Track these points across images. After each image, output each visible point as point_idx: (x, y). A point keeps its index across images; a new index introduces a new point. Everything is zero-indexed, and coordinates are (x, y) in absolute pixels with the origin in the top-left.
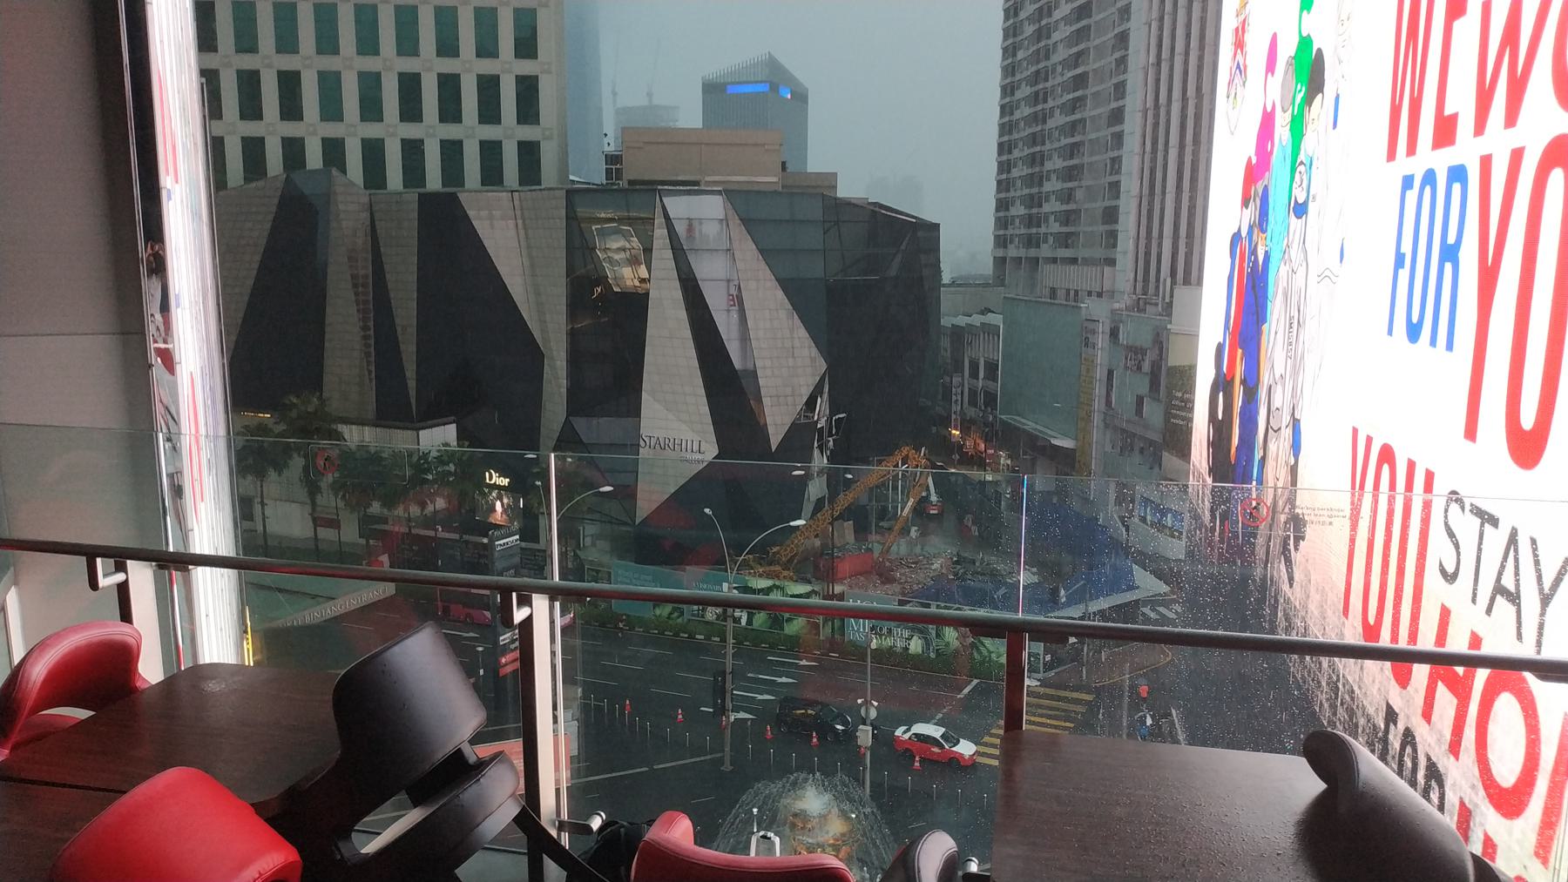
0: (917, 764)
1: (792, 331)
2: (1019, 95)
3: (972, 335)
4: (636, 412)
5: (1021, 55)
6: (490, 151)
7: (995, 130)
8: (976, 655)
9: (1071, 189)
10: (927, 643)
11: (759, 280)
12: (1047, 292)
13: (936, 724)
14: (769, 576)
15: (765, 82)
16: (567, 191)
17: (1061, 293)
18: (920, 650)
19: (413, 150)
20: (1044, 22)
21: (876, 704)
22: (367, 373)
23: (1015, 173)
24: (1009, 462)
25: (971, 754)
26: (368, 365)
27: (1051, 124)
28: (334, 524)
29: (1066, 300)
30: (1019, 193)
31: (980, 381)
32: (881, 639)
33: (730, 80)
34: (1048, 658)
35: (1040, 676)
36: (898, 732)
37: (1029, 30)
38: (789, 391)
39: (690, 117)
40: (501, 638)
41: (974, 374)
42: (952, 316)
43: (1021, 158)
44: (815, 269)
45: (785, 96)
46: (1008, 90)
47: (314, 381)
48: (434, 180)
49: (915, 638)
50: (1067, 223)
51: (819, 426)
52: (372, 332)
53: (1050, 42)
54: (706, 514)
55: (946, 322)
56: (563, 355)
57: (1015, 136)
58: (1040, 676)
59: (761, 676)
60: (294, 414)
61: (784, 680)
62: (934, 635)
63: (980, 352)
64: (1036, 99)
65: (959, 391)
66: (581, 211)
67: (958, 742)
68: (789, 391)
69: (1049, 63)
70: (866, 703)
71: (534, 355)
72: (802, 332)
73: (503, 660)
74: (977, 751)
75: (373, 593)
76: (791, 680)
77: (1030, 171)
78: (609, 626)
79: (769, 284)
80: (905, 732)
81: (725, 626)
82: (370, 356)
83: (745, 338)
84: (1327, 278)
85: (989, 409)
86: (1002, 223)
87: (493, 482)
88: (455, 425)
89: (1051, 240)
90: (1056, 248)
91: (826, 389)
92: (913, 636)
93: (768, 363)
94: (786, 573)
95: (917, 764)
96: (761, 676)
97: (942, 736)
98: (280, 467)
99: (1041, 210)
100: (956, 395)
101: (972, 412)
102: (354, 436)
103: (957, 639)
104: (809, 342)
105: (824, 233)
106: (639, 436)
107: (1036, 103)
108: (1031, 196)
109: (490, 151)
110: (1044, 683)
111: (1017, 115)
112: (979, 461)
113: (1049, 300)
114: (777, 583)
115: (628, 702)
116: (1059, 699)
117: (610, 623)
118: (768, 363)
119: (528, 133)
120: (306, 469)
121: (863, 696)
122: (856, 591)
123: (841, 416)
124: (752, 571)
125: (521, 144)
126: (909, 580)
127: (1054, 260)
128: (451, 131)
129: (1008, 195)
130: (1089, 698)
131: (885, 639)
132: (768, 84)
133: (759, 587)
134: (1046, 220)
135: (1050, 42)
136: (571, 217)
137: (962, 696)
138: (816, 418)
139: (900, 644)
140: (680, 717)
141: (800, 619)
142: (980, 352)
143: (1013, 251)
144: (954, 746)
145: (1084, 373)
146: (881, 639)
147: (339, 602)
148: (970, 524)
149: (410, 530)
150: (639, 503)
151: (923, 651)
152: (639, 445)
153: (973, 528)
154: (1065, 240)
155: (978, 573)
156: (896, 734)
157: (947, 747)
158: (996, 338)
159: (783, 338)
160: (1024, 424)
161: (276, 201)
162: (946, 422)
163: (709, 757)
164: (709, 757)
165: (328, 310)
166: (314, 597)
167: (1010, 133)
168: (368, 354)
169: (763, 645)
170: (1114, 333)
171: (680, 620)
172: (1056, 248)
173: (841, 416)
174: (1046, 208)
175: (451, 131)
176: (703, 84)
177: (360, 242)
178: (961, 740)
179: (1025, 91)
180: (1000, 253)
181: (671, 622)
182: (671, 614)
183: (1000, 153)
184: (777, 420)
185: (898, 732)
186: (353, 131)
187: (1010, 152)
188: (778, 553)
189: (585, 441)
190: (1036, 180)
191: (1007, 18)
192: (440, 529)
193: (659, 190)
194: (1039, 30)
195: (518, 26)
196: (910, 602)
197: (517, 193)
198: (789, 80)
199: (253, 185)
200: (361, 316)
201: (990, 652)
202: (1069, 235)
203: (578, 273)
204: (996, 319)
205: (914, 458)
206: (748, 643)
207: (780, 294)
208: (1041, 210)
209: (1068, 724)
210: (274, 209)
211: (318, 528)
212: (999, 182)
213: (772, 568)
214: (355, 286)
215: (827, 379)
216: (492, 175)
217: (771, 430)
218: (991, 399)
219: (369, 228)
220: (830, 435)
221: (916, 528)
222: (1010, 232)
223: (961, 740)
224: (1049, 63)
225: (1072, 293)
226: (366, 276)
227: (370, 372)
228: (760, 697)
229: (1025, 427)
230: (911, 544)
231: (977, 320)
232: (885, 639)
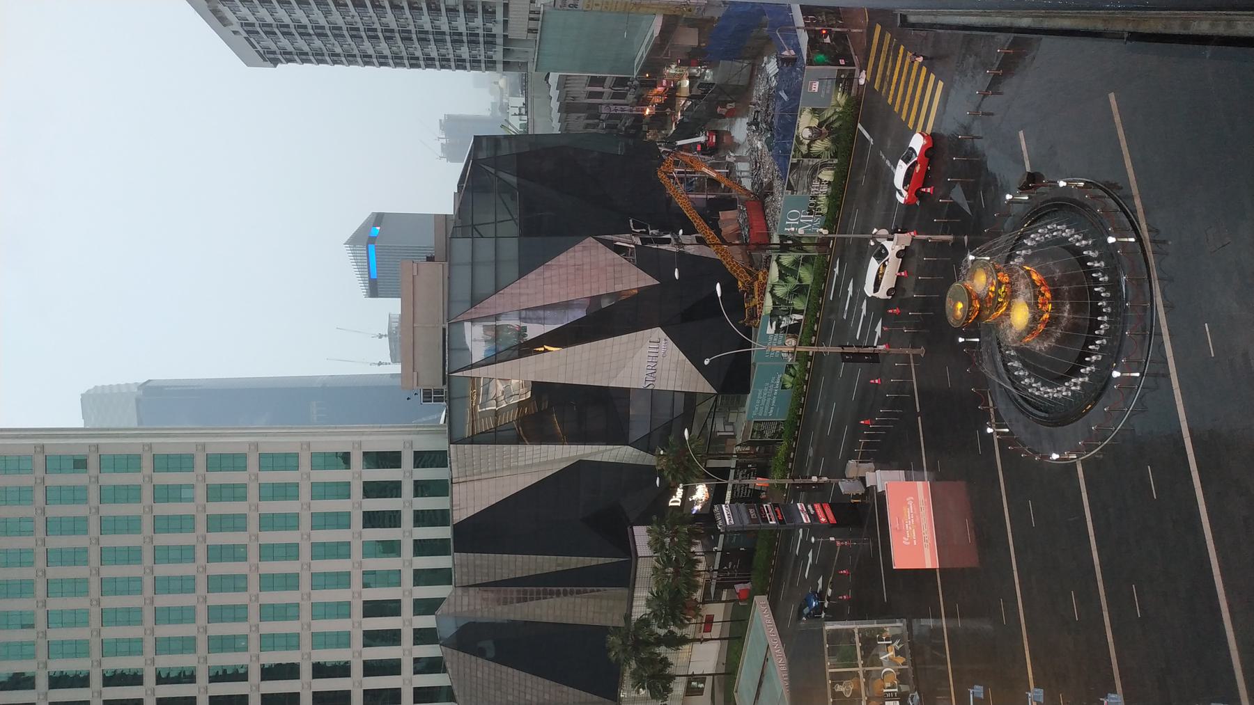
0: (929, 190)
1: (560, 266)
2: (371, 51)
3: (566, 84)
4: (625, 392)
5: (338, 50)
6: (422, 488)
7: (400, 70)
8: (836, 125)
9: (446, 9)
10: (824, 165)
11: (520, 294)
12: (531, 36)
13: (895, 168)
14: (762, 294)
15: (367, 249)
16: (451, 444)
17: (533, 25)
18: (831, 172)
19: (422, 547)
20: (311, 32)
21: (875, 230)
22: (593, 593)
23: (434, 54)
24: (673, 66)
25: (922, 138)
26: (587, 593)
27: (393, 25)
28: (710, 621)
29: (539, 14)
30: (451, 51)
31: (605, 90)
32: (819, 205)
33: (367, 276)
34: (842, 62)
35: (857, 68)
36: (901, 200)
37: (317, 43)
38: (610, 269)
39: (392, 306)
40: (805, 521)
41: (600, 95)
42: (550, 123)
43: (422, 50)
44: (511, 247)
45: (378, 232)
46: (367, 60)
47: (599, 632)
48: (444, 533)
49: (820, 176)
50: (474, 12)
51: (640, 243)
52: (561, 589)
53: (327, 26)
54: (709, 363)
55: (556, 128)
56: (581, 447)
57: (404, 54)
58: (857, 68)
59: (846, 308)
60: (622, 656)
61: (850, 289)
62: (818, 160)
63: (580, 90)
64: (373, 38)
65: (613, 108)
66: (468, 433)
67: (911, 149)
68: (610, 269)
69: (344, 27)
70: (874, 239)
71: (580, 466)
72: (562, 258)
73: (823, 520)
74: (920, 133)
75: (765, 614)
76: (851, 284)
77: (432, 42)
78: (798, 424)
79: (524, 285)
80: (901, 194)
81: (789, 484)
82: (580, 590)
83: (567, 305)
84: (451, 326)
85: (629, 83)
86: (475, 64)
87: (680, 501)
88: (634, 528)
89: (489, 25)
90: (495, 21)
91: (608, 237)
92: (819, 179)
93: (587, 286)
94: (761, 277)
95: (929, 190)
96: (846, 308)
97: (906, 163)
98: (665, 663)
99: (464, 34)
100: (616, 110)
101: (631, 97)
102: (640, 609)
103: (822, 141)
104: (570, 253)
105: (483, 237)
106: (645, 390)
107: (377, 37)
108: (453, 41)
109: (422, 488)
110: (864, 67)
111: (387, 52)
112: (672, 93)
113: (538, 35)
114: (775, 259)
115: (862, 422)
116: (879, 51)
117: (796, 423)
118: (587, 286)
119: (407, 460)
120: (668, 645)
121: (867, 240)
122: (778, 227)
123: (632, 224)
124: (758, 306)
125: (417, 465)
126: (770, 171)
127: (506, 22)
128: (407, 518)
129: (452, 60)
130: (878, 28)
131: (820, 201)
132: (369, 245)
133: (772, 304)
134: (473, 29)
135: (327, 26)
136: (472, 440)
137: (872, 140)
138: (633, 246)
139: (825, 189)
140: (877, 381)
141: (799, 271)
142: (580, 90)
143: (498, 55)
144: (915, 152)
145: (599, 8)
146: (819, 205)
147: (771, 643)
148: (725, 110)
149: (716, 570)
150: (699, 390)
151: (831, 169)
152: (652, 390)
153: (729, 107)
154: (489, 12)
155: (766, 110)
156: (903, 202)
157: (916, 159)
158: (569, 78)
159: (567, 273)
160: (642, 56)
161: (461, 654)
162: (639, 118)
163: (912, 364)
164: (912, 364)
165: (544, 620)
166: (766, 659)
167: (402, 58)
168: (578, 592)
169: (820, 301)
171: (796, 368)
172: (495, 21)
173: (632, 224)
174: (462, 29)
175: (407, 518)
176: (371, 297)
177: (491, 595)
178: (910, 146)
179: (367, 46)
180: (500, 66)
181: (798, 376)
182: (791, 375)
183: (418, 66)
184: (635, 279)
185: (901, 200)
186: (409, 562)
187: (417, 58)
188: (743, 283)
189: (648, 432)
190: (439, 37)
191: (309, 61)
192: (716, 548)
193: (449, 373)
194: (319, 35)
195: (326, 467)
196: (789, 180)
197: (453, 480)
198: (365, 228)
199: (448, 665)
200: (549, 596)
201: (835, 112)
202: (485, 11)
203: (516, 426)
204: (554, 78)
205: (668, 167)
206: (818, 314)
207: (531, 276)
208: (464, 34)
209: (901, 50)
210: (467, 656)
211: (712, 677)
212: (442, 67)
213: (756, 289)
214: (525, 600)
215: (598, 237)
216: (440, 488)
217: (642, 284)
218: (621, 82)
219: (481, 588)
220: (647, 233)
221: (727, 157)
222: (482, 58)
223: (910, 146)
224: (344, 27)
225: (532, 16)
226: (518, 592)
227: (593, 591)
228: (864, 312)
229: (644, 56)
230: (740, 159)
231: (554, 93)
232: (820, 201)
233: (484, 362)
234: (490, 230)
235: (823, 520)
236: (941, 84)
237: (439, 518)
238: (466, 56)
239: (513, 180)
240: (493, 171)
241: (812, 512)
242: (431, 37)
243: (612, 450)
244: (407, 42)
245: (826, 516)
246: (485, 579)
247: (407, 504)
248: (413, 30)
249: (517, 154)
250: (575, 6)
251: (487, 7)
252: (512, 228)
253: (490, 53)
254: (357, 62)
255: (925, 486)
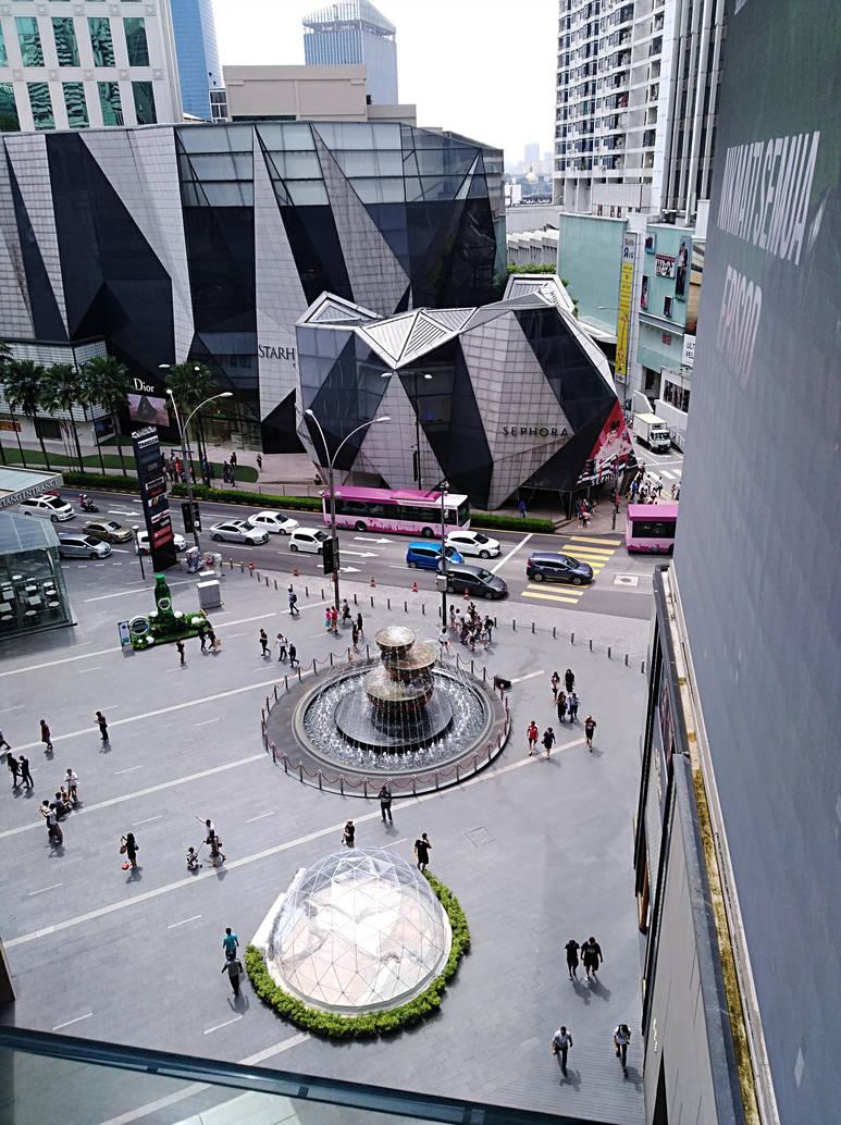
17: (607, 210)
27: (602, 54)
44: (394, 195)
55: (512, 237)
71: (166, 279)
170: (649, 243)
202: (615, 157)
204: (554, 235)
222: (567, 155)
228: (364, 555)
233: (665, 660)
234: (411, 170)
235: (156, 535)
236: (575, 601)
237: (77, 112)
238: (570, 138)
239: (463, 195)
240: (471, 172)
241: (163, 524)
242: (589, 98)
243: (188, 314)
244: (582, 71)
245: (160, 538)
246: (17, 173)
247: (88, 72)
248: (596, 77)
249: (488, 198)
250: (626, 255)
251: (619, 159)
252: (414, 193)
253: (572, 163)
254: (563, 11)
255: (210, 510)
